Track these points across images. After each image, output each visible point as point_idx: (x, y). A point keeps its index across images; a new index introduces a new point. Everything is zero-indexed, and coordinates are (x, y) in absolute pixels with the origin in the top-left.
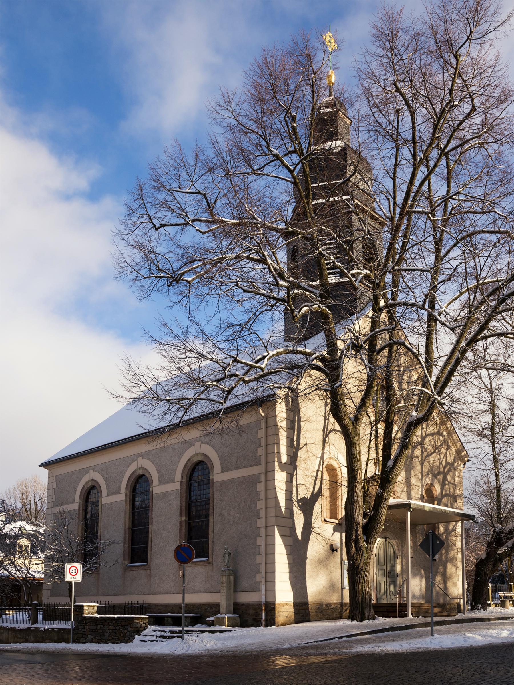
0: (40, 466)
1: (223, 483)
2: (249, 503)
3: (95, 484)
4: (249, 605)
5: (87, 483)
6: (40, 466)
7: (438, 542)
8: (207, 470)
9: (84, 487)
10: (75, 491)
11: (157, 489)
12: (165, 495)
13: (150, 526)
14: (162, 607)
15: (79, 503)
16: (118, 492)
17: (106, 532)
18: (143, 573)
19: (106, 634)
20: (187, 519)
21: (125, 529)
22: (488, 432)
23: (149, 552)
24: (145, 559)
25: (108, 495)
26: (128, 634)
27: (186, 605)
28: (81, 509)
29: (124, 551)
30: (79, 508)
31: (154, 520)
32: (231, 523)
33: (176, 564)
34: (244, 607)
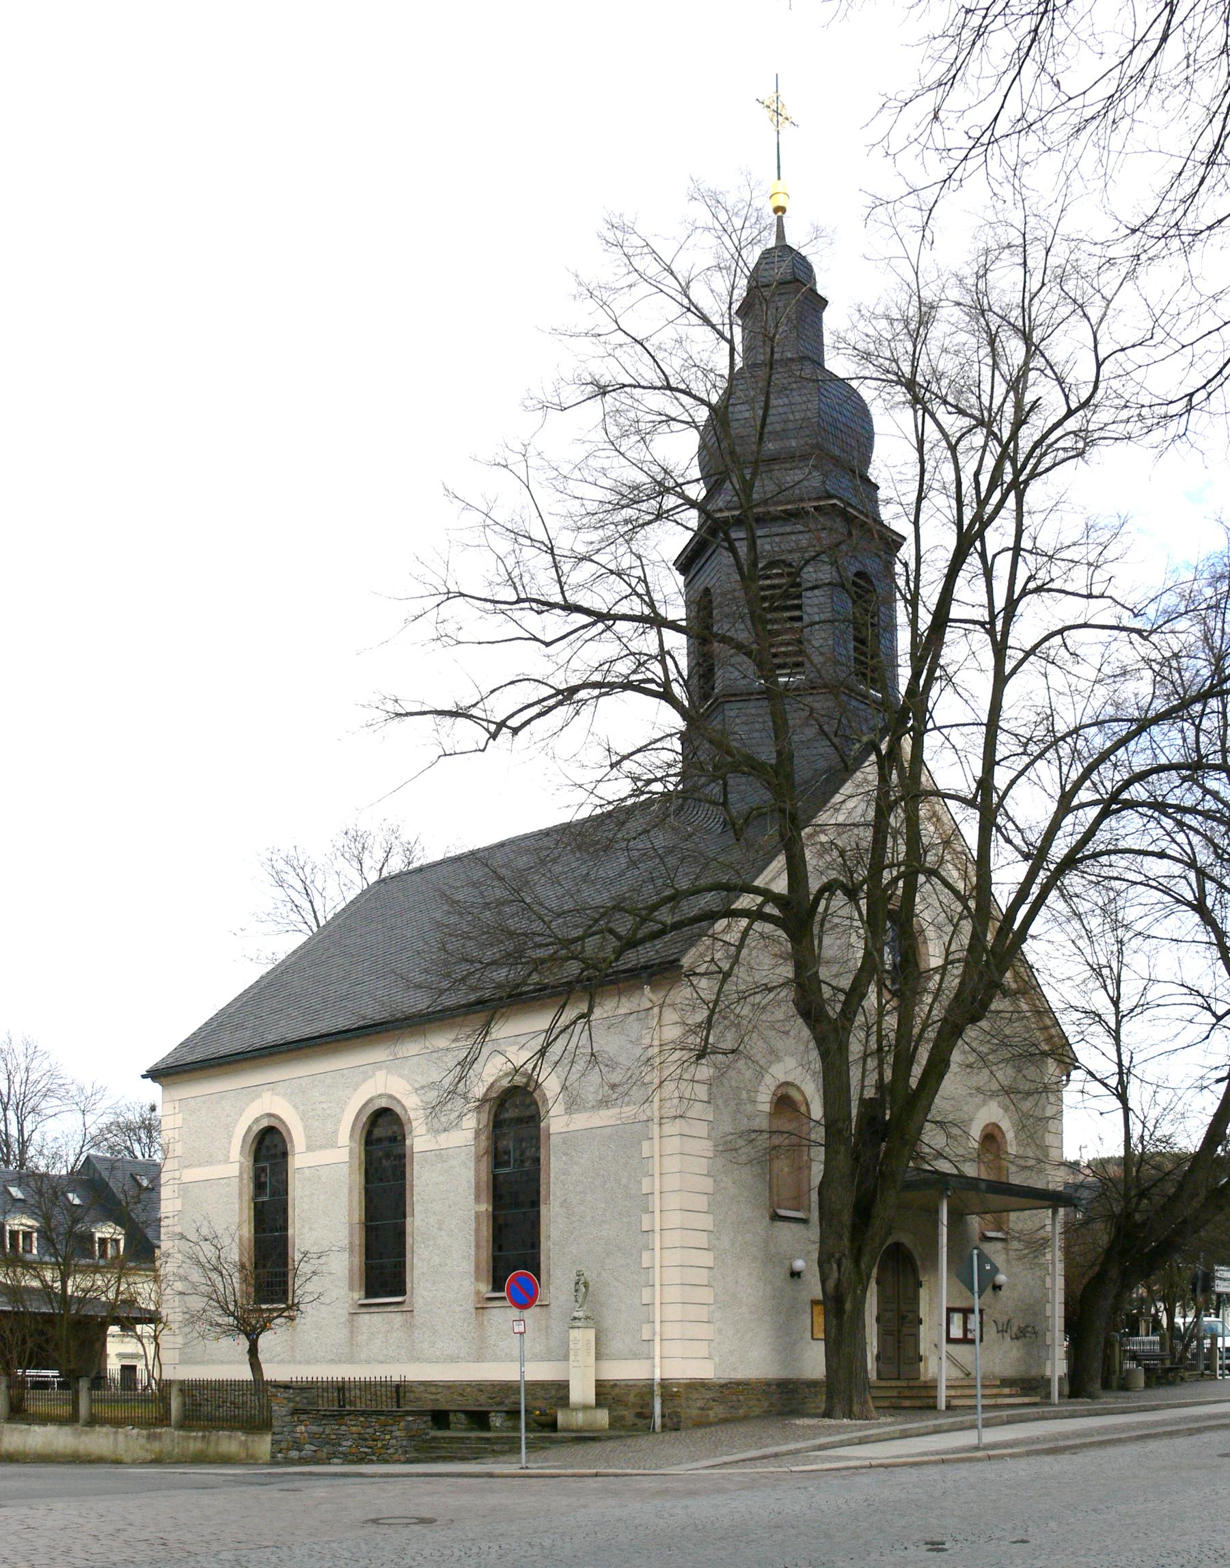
0: (144, 1077)
1: (567, 1136)
2: (624, 1181)
3: (274, 1123)
4: (629, 1385)
5: (257, 1120)
6: (144, 1077)
7: (988, 1268)
8: (533, 1107)
9: (250, 1128)
10: (230, 1137)
11: (420, 1141)
12: (440, 1155)
13: (409, 1220)
14: (440, 1390)
15: (241, 1164)
16: (331, 1143)
17: (306, 1230)
18: (398, 1319)
19: (345, 1443)
20: (490, 1209)
21: (351, 1225)
22: (492, 728)
23: (408, 1274)
24: (398, 1286)
25: (309, 1148)
26: (393, 1442)
27: (528, 1384)
28: (245, 1176)
29: (350, 1271)
30: (241, 1173)
31: (417, 1208)
32: (588, 1219)
33: (358, 1295)
34: (617, 1390)
